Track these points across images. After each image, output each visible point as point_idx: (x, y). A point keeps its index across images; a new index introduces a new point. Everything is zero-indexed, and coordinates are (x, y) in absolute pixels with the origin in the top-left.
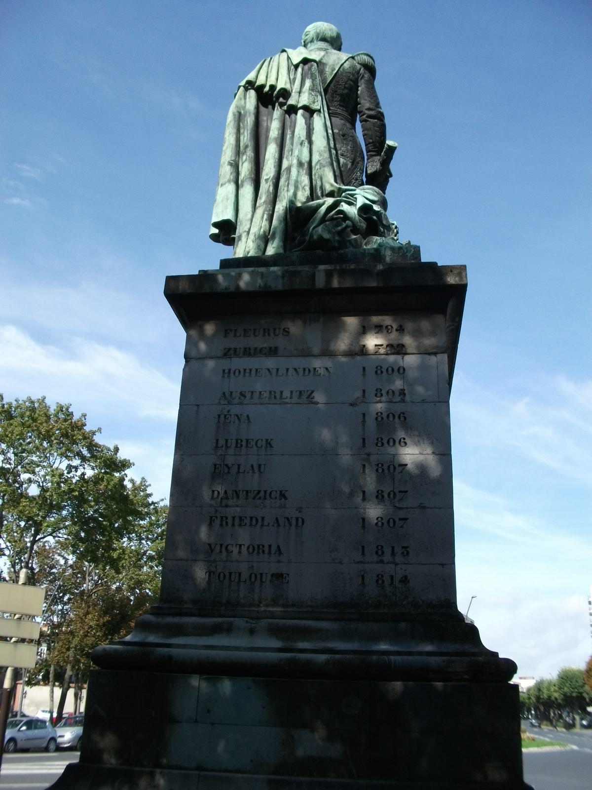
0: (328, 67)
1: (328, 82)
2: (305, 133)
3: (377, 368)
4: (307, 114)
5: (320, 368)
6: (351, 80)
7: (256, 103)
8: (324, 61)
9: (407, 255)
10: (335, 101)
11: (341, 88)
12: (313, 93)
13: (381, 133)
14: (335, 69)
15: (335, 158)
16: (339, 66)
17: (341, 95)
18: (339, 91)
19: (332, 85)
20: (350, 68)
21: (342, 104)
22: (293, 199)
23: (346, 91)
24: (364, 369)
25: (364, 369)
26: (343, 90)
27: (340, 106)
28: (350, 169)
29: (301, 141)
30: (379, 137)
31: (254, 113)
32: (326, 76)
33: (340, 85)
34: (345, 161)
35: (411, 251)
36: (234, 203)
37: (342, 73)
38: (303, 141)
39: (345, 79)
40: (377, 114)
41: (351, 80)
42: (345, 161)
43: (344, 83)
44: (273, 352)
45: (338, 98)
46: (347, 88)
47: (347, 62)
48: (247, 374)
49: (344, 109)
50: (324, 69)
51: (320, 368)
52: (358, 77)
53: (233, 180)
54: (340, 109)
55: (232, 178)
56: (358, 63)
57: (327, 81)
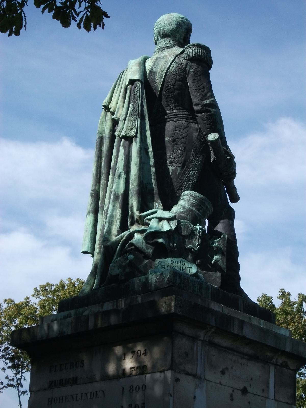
0: (157, 74)
1: (159, 89)
2: (123, 164)
3: (130, 387)
4: (127, 143)
5: (99, 391)
6: (179, 80)
7: (111, 125)
8: (154, 70)
9: (165, 280)
10: (170, 104)
11: (171, 91)
12: (132, 119)
13: (210, 124)
14: (163, 75)
15: (154, 176)
16: (165, 71)
17: (173, 97)
18: (171, 95)
19: (164, 91)
20: (175, 69)
21: (177, 104)
22: (107, 236)
23: (177, 92)
24: (123, 388)
25: (123, 388)
26: (174, 92)
27: (176, 106)
28: (180, 173)
29: (119, 173)
30: (209, 129)
31: (109, 137)
32: (157, 85)
33: (170, 88)
34: (174, 168)
35: (167, 275)
36: (91, 234)
37: (169, 77)
38: (121, 172)
39: (173, 82)
40: (203, 108)
41: (179, 80)
42: (174, 168)
43: (173, 86)
44: (74, 381)
45: (172, 101)
46: (177, 89)
47: (173, 63)
48: (61, 401)
49: (181, 108)
50: (155, 78)
51: (99, 391)
52: (186, 73)
53: (91, 211)
54: (176, 110)
55: (91, 208)
56: (185, 59)
57: (158, 89)
